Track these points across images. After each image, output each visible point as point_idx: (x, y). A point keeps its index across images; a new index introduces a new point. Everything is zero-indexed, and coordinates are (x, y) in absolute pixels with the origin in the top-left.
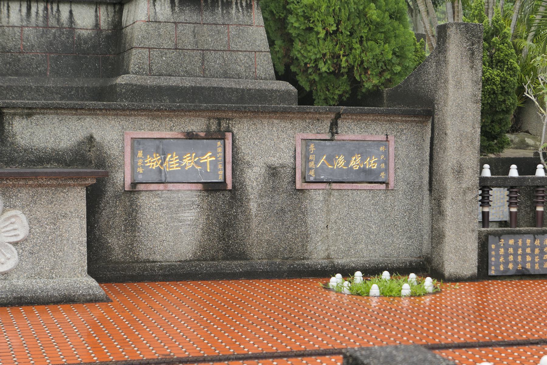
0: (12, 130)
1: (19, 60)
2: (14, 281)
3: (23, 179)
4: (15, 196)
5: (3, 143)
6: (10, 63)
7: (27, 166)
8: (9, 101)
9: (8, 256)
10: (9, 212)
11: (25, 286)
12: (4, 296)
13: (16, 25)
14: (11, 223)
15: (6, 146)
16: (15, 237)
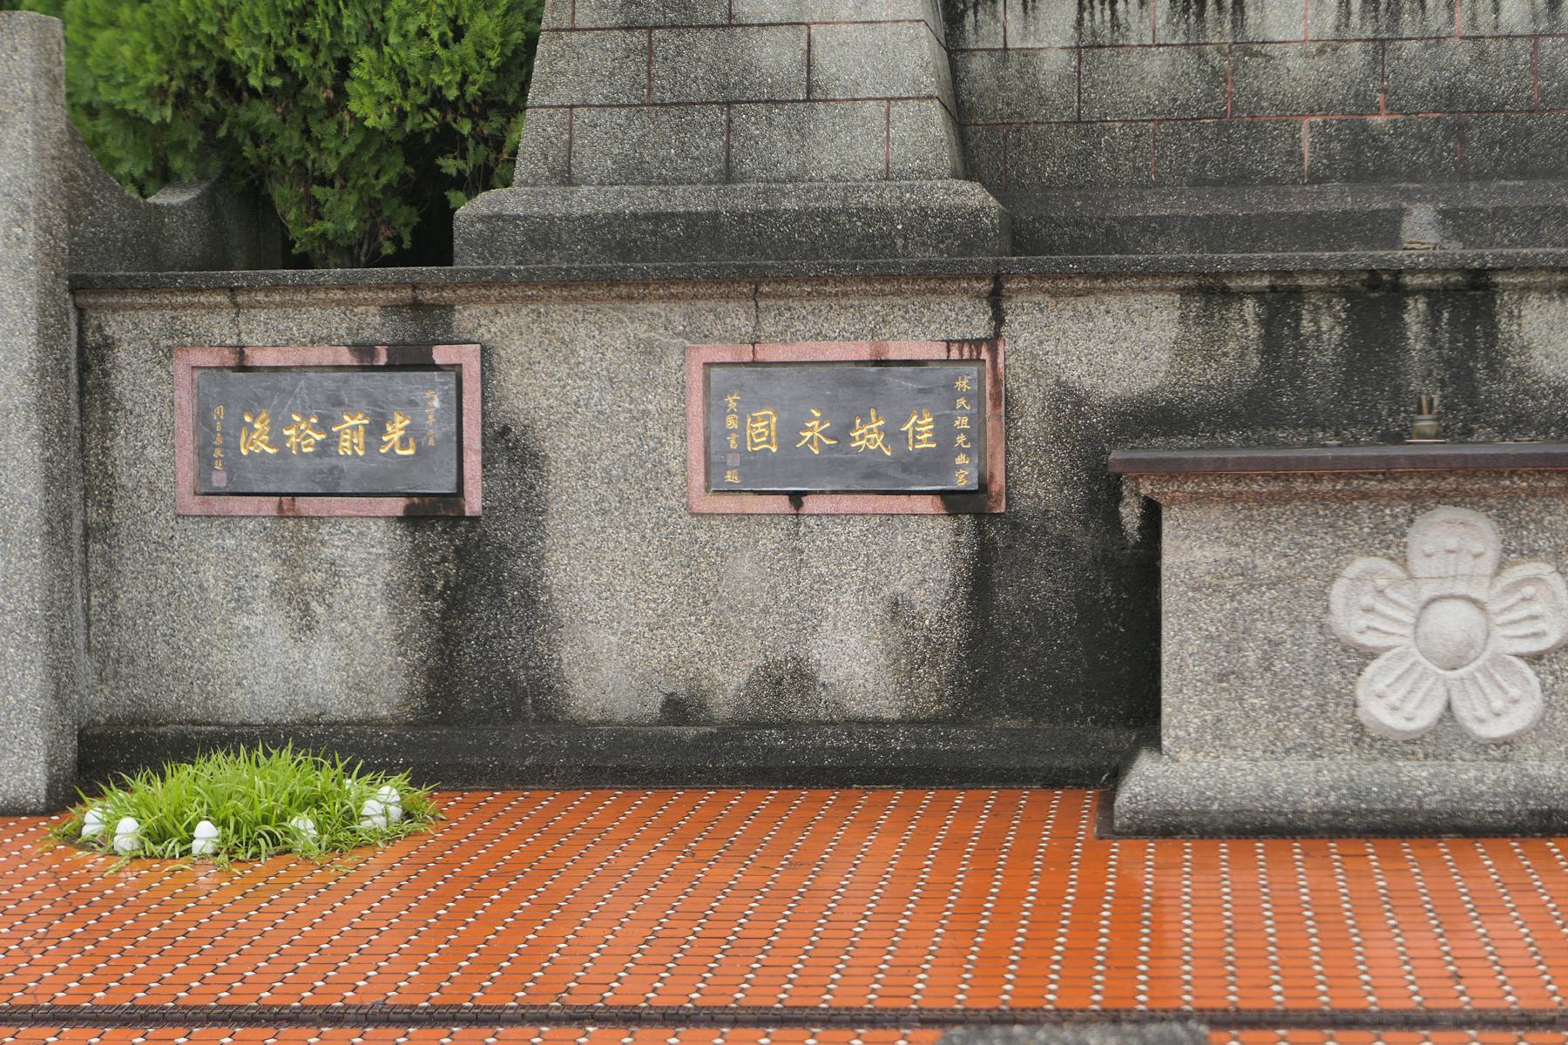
0: (1518, 332)
1: (1529, 133)
2: (1531, 766)
3: (1559, 473)
4: (1533, 521)
5: (1495, 371)
6: (1502, 143)
7: (1561, 436)
8: (1511, 251)
9: (1515, 692)
10: (1517, 568)
11: (1561, 780)
12: (1501, 807)
13: (1518, 30)
14: (1524, 600)
15: (1502, 378)
16: (1532, 640)
